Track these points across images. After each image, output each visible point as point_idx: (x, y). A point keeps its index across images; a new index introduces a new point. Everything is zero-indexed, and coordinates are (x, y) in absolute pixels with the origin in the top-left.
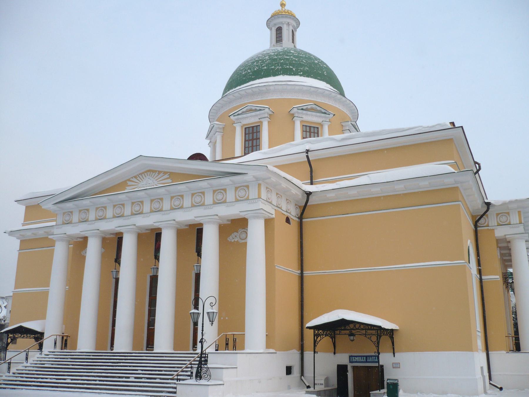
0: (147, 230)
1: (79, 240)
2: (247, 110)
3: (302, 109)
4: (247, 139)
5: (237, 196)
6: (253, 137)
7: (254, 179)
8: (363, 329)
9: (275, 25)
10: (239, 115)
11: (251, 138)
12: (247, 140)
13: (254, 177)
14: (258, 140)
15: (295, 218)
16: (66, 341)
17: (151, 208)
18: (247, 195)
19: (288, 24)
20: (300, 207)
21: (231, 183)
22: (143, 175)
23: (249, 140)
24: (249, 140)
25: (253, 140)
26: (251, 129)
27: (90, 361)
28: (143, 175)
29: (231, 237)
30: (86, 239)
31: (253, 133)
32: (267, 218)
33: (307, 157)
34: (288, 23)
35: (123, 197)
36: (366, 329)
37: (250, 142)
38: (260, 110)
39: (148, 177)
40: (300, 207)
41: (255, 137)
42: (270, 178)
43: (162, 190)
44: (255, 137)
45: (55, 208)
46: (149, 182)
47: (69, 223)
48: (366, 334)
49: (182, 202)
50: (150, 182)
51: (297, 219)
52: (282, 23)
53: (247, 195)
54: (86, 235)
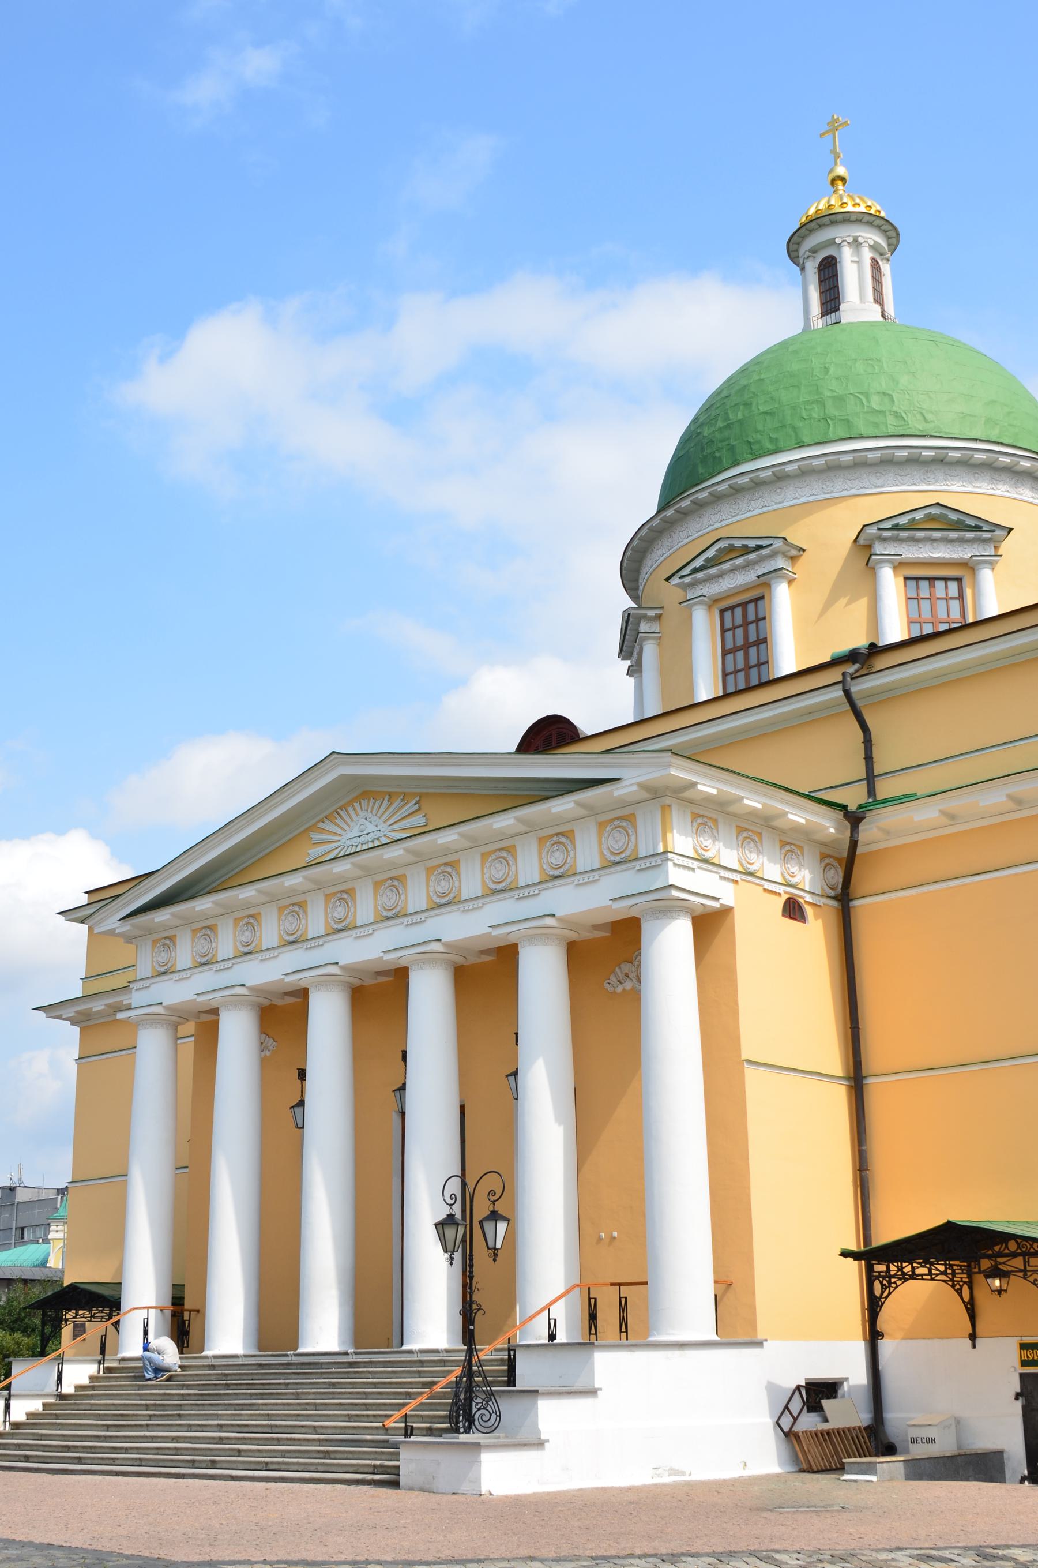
0: (596, 927)
1: (382, 979)
2: (719, 550)
3: (896, 527)
4: (729, 645)
5: (605, 852)
6: (933, 613)
7: (646, 795)
8: (1014, 1255)
9: (814, 251)
10: (696, 570)
11: (740, 642)
12: (753, 644)
13: (642, 786)
14: (762, 646)
15: (821, 901)
16: (183, 1320)
17: (376, 907)
18: (631, 846)
19: (856, 244)
20: (839, 860)
21: (582, 812)
22: (350, 809)
23: (735, 650)
24: (735, 650)
25: (747, 646)
26: (738, 611)
27: (227, 1380)
28: (350, 809)
29: (613, 980)
30: (401, 975)
31: (746, 624)
32: (699, 911)
33: (847, 693)
34: (855, 240)
35: (292, 881)
36: (1024, 1254)
37: (740, 655)
38: (759, 547)
39: (362, 814)
40: (839, 860)
41: (753, 638)
42: (695, 784)
43: (395, 853)
44: (753, 638)
45: (126, 927)
46: (363, 826)
47: (164, 972)
48: (1025, 1271)
49: (456, 884)
50: (371, 828)
51: (834, 903)
52: (832, 243)
53: (631, 846)
54: (403, 963)
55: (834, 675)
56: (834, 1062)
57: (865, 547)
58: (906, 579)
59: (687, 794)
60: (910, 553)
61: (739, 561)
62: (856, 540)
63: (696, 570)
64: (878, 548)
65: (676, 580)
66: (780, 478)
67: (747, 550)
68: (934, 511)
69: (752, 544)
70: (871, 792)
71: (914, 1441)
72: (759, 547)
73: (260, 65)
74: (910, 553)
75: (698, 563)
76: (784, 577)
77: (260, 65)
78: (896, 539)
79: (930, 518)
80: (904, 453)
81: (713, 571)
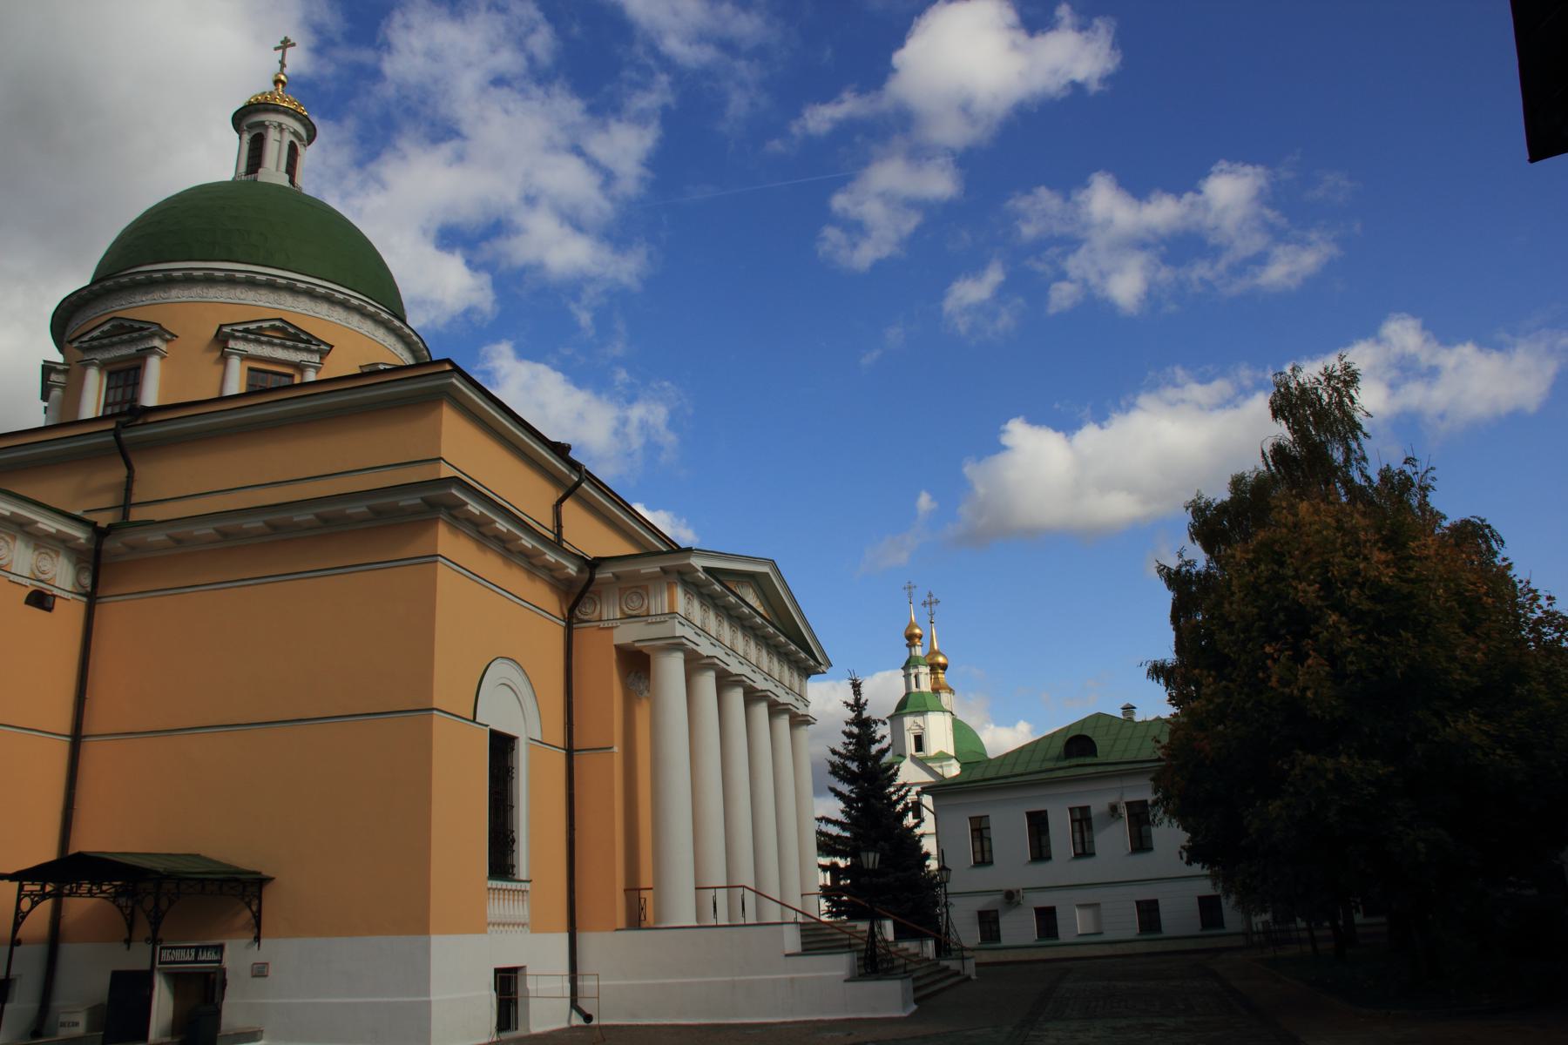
3: (247, 331)
4: (111, 400)
11: (119, 398)
38: (142, 329)
55: (111, 425)
56: (64, 724)
57: (221, 339)
58: (250, 369)
59: (455, 512)
60: (252, 349)
61: (125, 337)
62: (457, 370)
63: (93, 339)
64: (232, 344)
65: (76, 344)
66: (169, 281)
67: (134, 330)
68: (278, 323)
69: (137, 325)
70: (126, 515)
71: (63, 1025)
72: (142, 329)
73: (1344, 499)
74: (252, 349)
75: (96, 333)
76: (157, 353)
77: (1344, 499)
78: (245, 339)
79: (273, 328)
80: (264, 278)
81: (105, 341)
